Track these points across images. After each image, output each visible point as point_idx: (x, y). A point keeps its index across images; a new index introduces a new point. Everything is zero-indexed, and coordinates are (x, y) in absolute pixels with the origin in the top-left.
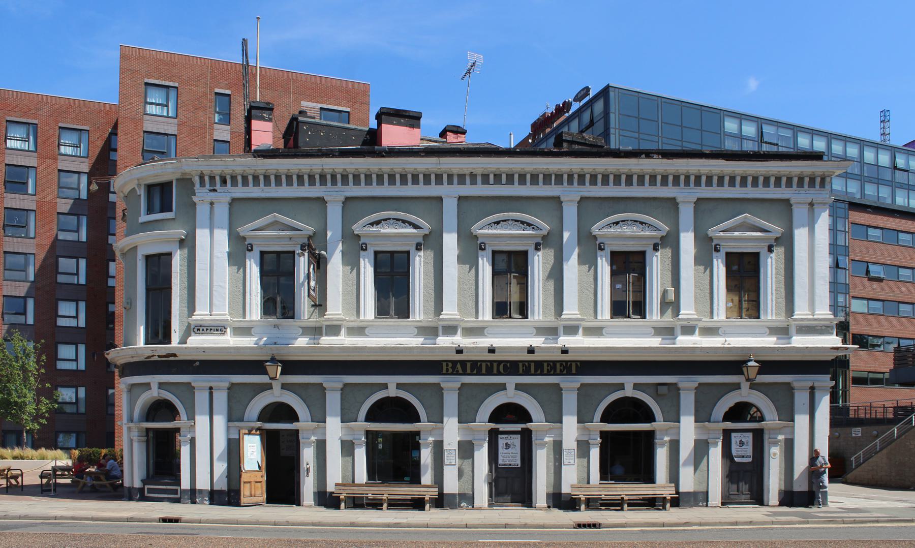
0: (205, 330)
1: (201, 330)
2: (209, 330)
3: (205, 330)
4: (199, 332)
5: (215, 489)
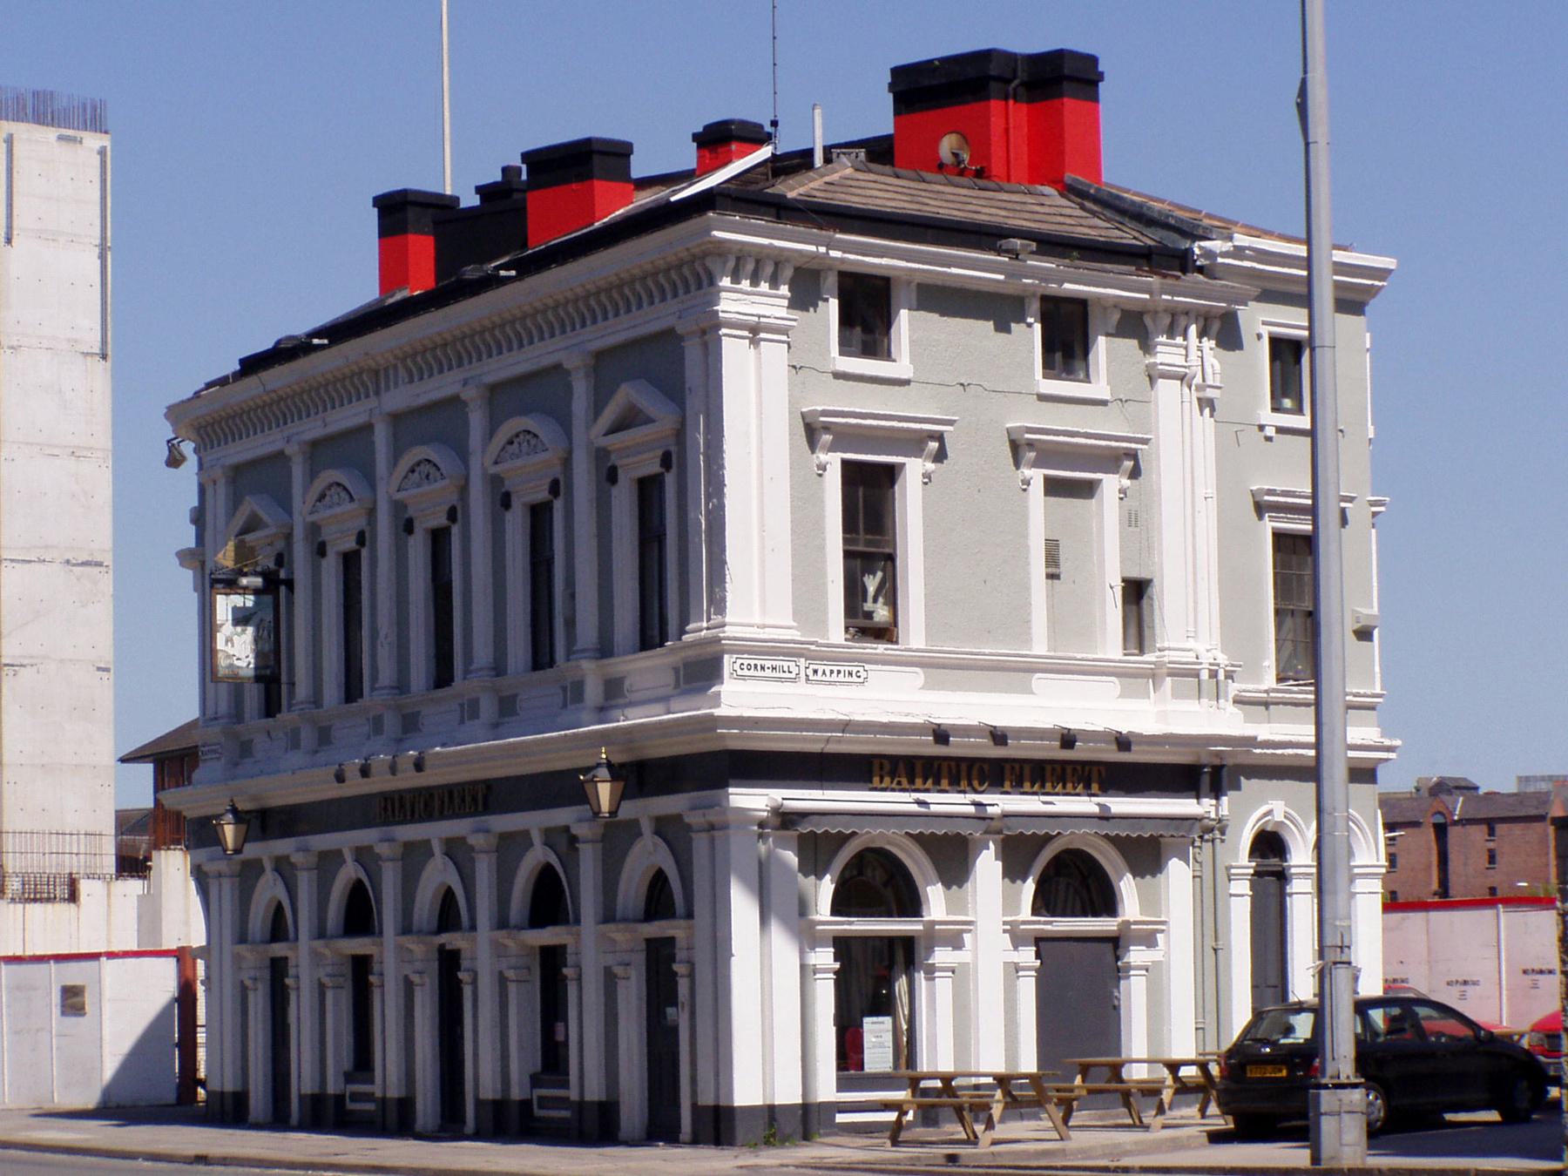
0: (828, 673)
1: (820, 673)
2: (836, 672)
3: (828, 673)
4: (815, 678)
5: (736, 1104)
